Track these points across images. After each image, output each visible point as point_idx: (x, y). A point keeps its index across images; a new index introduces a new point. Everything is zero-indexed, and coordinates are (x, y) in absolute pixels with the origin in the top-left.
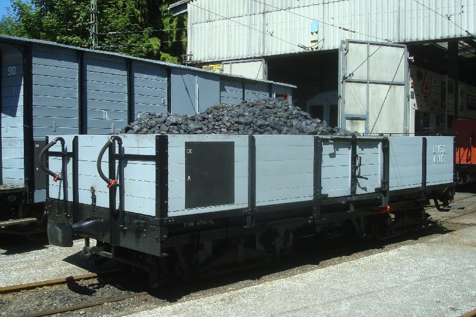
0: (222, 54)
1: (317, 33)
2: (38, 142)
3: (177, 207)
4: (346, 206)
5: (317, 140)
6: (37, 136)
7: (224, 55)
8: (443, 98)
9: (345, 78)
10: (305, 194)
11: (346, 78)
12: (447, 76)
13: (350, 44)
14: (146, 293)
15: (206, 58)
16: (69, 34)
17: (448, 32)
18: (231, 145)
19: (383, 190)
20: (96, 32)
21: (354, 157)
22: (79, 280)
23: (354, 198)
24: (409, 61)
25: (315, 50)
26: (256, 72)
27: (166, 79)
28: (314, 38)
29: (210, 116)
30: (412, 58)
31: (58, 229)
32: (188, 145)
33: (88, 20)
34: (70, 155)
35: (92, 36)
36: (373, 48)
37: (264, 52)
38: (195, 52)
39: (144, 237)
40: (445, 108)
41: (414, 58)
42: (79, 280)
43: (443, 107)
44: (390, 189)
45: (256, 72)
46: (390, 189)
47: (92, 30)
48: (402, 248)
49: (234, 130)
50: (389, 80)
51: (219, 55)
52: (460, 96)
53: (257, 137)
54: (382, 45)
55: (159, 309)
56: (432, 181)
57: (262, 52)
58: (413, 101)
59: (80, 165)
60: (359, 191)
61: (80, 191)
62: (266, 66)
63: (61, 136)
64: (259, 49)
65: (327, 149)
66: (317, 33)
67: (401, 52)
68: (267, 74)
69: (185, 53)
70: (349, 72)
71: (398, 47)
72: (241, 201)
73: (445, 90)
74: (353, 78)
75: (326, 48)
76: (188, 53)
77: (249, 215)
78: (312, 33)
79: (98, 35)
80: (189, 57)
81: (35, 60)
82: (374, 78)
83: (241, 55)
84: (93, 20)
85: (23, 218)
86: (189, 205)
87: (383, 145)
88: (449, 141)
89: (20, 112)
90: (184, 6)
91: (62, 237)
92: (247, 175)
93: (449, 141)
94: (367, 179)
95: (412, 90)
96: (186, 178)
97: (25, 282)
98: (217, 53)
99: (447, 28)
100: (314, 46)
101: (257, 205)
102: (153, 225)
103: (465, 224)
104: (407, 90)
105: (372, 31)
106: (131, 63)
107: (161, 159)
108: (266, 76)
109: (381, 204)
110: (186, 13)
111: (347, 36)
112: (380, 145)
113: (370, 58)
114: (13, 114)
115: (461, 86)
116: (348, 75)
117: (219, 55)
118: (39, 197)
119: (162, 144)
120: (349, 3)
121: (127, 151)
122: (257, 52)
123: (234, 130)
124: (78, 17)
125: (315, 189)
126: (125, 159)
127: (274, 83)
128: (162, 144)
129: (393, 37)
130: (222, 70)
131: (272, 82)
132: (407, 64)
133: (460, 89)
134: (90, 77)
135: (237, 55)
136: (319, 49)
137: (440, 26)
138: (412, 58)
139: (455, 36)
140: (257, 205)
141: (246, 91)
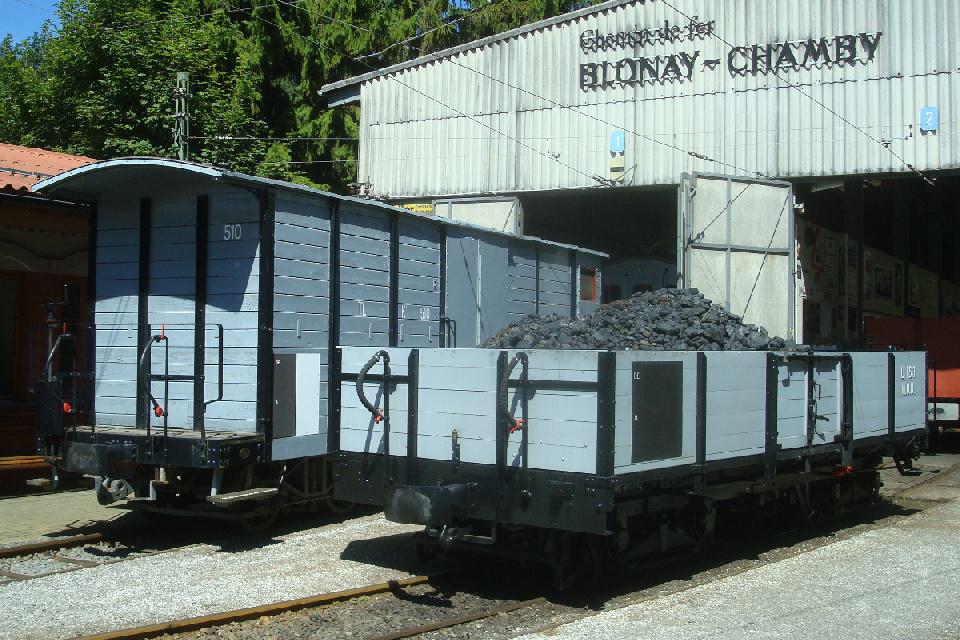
0: (417, 186)
1: (622, 154)
2: (281, 357)
3: (624, 463)
4: (800, 465)
5: (770, 357)
6: (278, 341)
7: (436, 188)
8: (842, 280)
9: (691, 241)
10: (361, 449)
11: (692, 242)
12: (846, 235)
13: (699, 181)
14: (543, 599)
15: (399, 191)
16: (125, 135)
17: (868, 161)
18: (680, 364)
19: (844, 438)
20: (185, 133)
21: (812, 385)
22: (405, 586)
23: (813, 451)
24: (796, 212)
25: (618, 184)
26: (502, 218)
27: (439, 245)
28: (617, 162)
29: (614, 319)
30: (801, 206)
31: (424, 497)
32: (637, 366)
33: (168, 110)
34: (400, 379)
35: (178, 142)
36: (737, 188)
37: (517, 186)
38: (375, 179)
39: (571, 507)
40: (844, 293)
41: (805, 207)
42: (405, 586)
43: (842, 293)
44: (855, 437)
45: (502, 218)
46: (855, 437)
47: (178, 133)
48: (270, 602)
49: (657, 343)
50: (762, 245)
51: (426, 187)
52: (865, 274)
53: (713, 356)
54: (749, 182)
55: (588, 619)
56: (901, 426)
57: (513, 185)
58: (800, 283)
59: (422, 397)
60: (817, 440)
61: (420, 439)
62: (520, 211)
63: (386, 349)
64: (508, 179)
65: (783, 372)
66: (622, 154)
67: (783, 197)
68: (522, 225)
69: (355, 179)
70: (697, 230)
71: (769, 185)
72: (688, 456)
73: (844, 260)
74: (705, 241)
75: (640, 182)
76: (361, 179)
77: (698, 474)
78: (613, 154)
79: (190, 141)
80: (362, 189)
81: (279, 216)
82: (737, 242)
83: (462, 188)
84: (180, 110)
85: (253, 486)
86: (636, 459)
87: (843, 368)
88: (920, 357)
89: (251, 300)
90: (355, 89)
91: (432, 510)
92: (695, 413)
93: (920, 357)
94: (828, 420)
95: (798, 262)
96: (634, 417)
97: (337, 590)
98: (422, 177)
99: (865, 156)
100: (615, 176)
101: (708, 458)
102: (592, 487)
103: (930, 501)
104: (791, 263)
105: (727, 153)
106: (397, 219)
107: (604, 388)
108: (520, 229)
109: (839, 461)
110: (357, 103)
111: (702, 167)
112: (838, 366)
113: (733, 206)
114: (233, 304)
115: (868, 254)
116: (695, 237)
117: (426, 187)
118: (281, 451)
119: (607, 366)
120: (493, 53)
121: (533, 376)
122: (501, 183)
123: (657, 343)
124: (150, 104)
125: (768, 437)
126: (527, 388)
127: (539, 239)
128: (607, 366)
129: (767, 167)
130: (433, 213)
131: (576, 248)
132: (792, 215)
133: (865, 259)
134: (345, 243)
135: (470, 188)
136: (627, 184)
137: (853, 155)
138: (801, 206)
139: (880, 169)
140: (708, 458)
141: (541, 264)
